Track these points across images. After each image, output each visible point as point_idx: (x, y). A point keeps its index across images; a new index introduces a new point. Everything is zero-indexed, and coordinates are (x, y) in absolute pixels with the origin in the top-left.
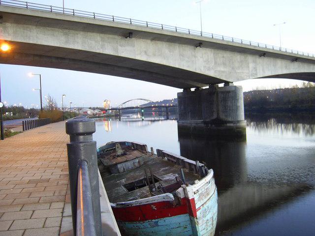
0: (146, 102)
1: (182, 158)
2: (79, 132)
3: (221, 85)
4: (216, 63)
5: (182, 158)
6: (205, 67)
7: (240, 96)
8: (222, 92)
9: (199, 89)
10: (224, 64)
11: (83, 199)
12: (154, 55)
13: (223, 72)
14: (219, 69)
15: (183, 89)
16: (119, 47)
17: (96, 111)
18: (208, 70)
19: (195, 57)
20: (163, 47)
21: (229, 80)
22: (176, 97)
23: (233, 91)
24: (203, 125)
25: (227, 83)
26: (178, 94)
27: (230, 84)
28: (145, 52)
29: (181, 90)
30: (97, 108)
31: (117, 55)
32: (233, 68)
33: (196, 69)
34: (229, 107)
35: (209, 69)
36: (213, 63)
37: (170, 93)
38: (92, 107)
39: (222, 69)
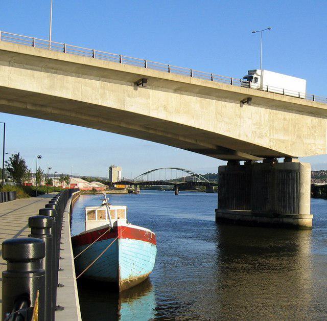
0: (186, 175)
1: (131, 226)
2: (122, 304)
3: (281, 160)
4: (272, 127)
5: (131, 226)
6: (254, 132)
7: (305, 181)
8: (281, 171)
9: (250, 164)
10: (285, 130)
11: (44, 302)
12: (178, 112)
13: (283, 141)
14: (276, 136)
15: (279, 162)
16: (127, 98)
17: (94, 185)
18: (259, 137)
19: (240, 117)
20: (193, 101)
21: (290, 154)
22: (216, 172)
23: (295, 171)
24: (221, 214)
25: (288, 158)
26: (220, 167)
27: (293, 160)
28: (165, 107)
29: (225, 163)
30: (98, 180)
31: (122, 109)
32: (299, 137)
33: (239, 135)
34: (289, 194)
35: (261, 137)
36: (268, 128)
37: (210, 165)
38: (87, 175)
39: (281, 136)
